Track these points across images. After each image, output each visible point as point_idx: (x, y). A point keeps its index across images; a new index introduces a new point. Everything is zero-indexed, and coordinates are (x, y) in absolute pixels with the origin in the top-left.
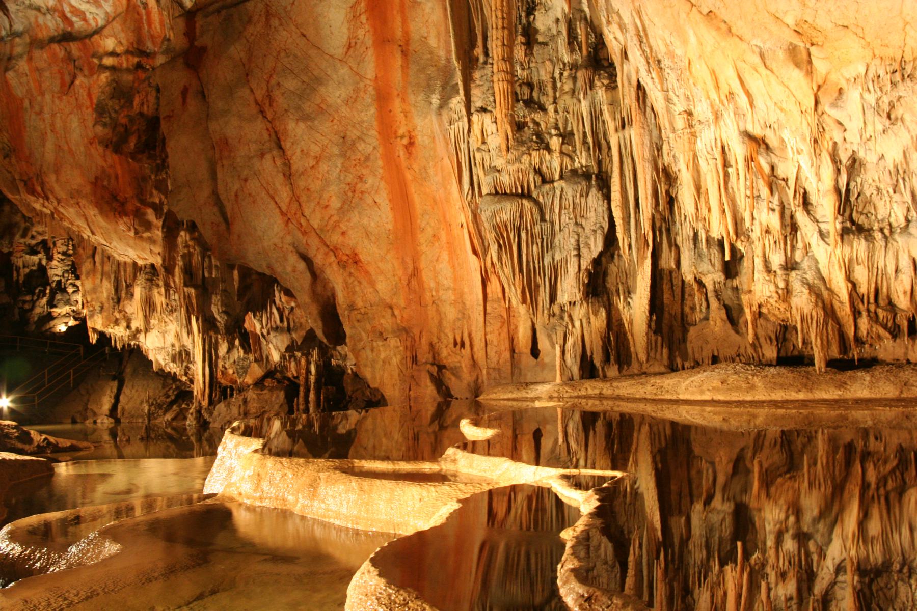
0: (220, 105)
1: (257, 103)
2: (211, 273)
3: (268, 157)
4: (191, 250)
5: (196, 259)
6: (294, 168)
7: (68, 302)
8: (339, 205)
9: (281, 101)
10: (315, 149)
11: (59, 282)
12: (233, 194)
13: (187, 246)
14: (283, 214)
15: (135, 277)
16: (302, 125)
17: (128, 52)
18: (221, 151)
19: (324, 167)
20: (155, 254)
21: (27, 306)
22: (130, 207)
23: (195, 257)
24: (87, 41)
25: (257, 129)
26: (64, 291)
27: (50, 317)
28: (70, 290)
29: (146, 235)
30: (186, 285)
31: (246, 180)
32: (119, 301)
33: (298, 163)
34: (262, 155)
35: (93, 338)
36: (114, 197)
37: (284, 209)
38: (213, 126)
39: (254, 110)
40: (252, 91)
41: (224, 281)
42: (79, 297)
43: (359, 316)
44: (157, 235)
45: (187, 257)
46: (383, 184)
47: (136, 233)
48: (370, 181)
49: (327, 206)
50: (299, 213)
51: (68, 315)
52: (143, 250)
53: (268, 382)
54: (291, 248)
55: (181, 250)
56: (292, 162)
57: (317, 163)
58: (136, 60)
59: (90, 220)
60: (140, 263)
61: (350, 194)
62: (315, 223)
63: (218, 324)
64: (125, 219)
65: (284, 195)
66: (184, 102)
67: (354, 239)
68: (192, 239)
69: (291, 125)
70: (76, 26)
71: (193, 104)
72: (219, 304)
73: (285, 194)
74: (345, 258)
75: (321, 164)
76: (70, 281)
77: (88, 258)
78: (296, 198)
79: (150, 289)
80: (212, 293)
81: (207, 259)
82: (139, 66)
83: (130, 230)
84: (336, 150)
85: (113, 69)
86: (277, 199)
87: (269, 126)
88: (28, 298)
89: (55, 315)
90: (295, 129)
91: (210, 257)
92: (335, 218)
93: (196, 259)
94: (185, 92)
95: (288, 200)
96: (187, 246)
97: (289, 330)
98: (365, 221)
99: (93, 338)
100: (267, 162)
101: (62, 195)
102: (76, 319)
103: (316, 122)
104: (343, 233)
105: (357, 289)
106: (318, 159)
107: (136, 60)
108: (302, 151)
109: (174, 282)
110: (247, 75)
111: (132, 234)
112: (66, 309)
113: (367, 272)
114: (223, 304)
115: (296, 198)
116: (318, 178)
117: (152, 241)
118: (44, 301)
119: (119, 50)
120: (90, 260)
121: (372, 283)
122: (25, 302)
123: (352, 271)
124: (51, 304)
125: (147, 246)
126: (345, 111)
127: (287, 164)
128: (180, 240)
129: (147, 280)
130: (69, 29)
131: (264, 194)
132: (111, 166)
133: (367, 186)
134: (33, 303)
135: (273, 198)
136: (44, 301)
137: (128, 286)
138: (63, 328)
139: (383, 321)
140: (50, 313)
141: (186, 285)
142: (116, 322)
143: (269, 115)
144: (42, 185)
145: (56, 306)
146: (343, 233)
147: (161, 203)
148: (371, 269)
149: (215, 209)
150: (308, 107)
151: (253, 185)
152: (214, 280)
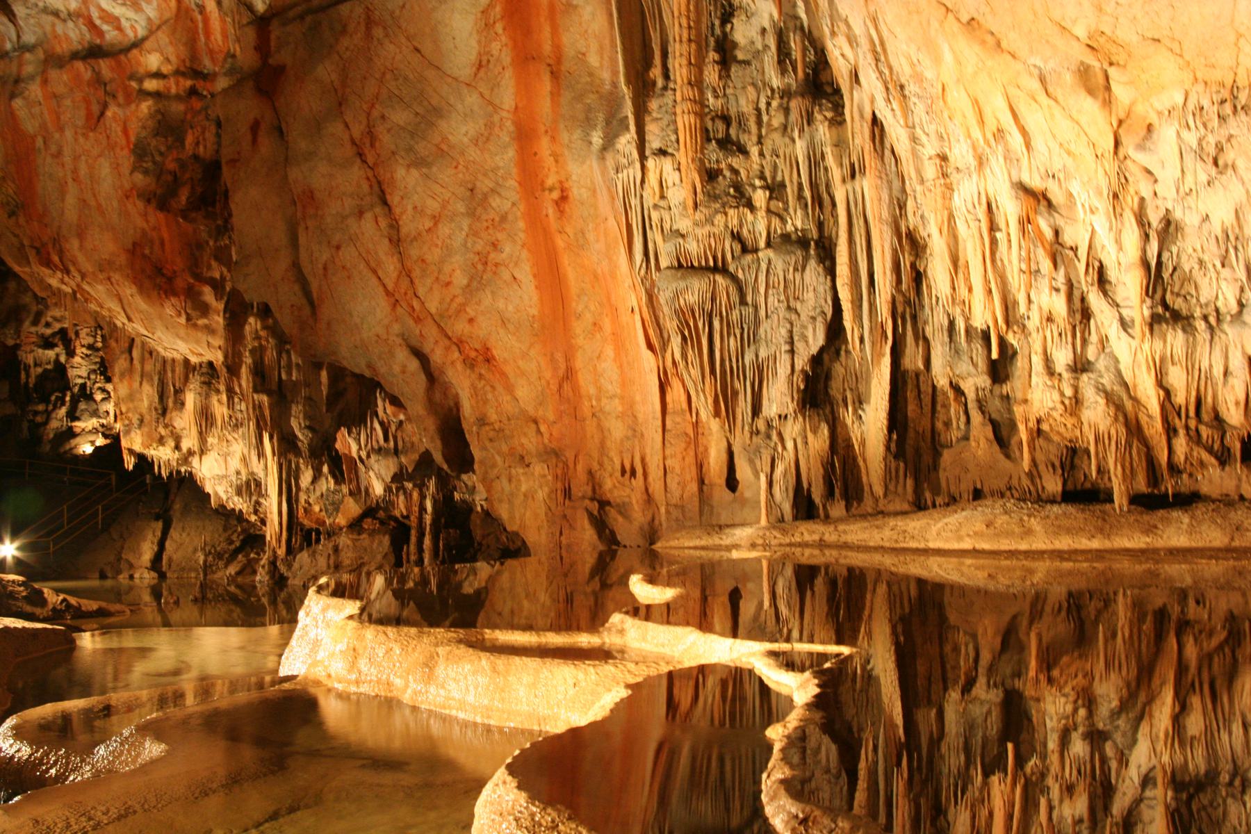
0: (303, 145)
1: (353, 142)
2: (289, 374)
3: (368, 216)
4: (264, 343)
5: (270, 355)
6: (404, 231)
7: (95, 414)
8: (465, 282)
9: (386, 140)
10: (433, 206)
11: (83, 386)
12: (320, 266)
13: (258, 338)
14: (388, 293)
15: (186, 379)
16: (415, 172)
17: (177, 73)
18: (304, 207)
19: (444, 230)
20: (214, 347)
21: (39, 419)
22: (180, 283)
23: (269, 352)
24: (122, 57)
25: (353, 178)
26: (90, 398)
27: (71, 434)
28: (99, 396)
29: (202, 322)
30: (256, 391)
31: (338, 248)
32: (164, 412)
33: (409, 225)
34: (361, 214)
35: (130, 463)
36: (159, 270)
37: (390, 287)
38: (294, 173)
39: (349, 151)
40: (347, 126)
41: (308, 385)
42: (110, 407)
43: (492, 434)
44: (218, 322)
45: (258, 353)
46: (525, 254)
47: (189, 319)
48: (508, 249)
49: (448, 284)
50: (410, 293)
51: (95, 431)
52: (198, 342)
53: (368, 523)
54: (399, 341)
55: (250, 343)
56: (401, 223)
57: (436, 224)
58: (189, 83)
59: (125, 301)
60: (194, 360)
61: (480, 267)
62: (433, 307)
63: (300, 444)
64: (174, 300)
65: (390, 267)
66: (254, 141)
67: (485, 328)
68: (264, 328)
69: (400, 172)
70: (108, 37)
71: (267, 145)
72: (301, 416)
73: (392, 268)
74: (473, 354)
75: (440, 226)
76: (97, 385)
77: (122, 352)
78: (405, 272)
79: (207, 396)
80: (292, 402)
81: (284, 356)
82: (193, 92)
83: (179, 315)
84: (461, 207)
85: (157, 95)
86: (380, 273)
87: (370, 174)
88: (41, 407)
89: (77, 430)
90: (405, 178)
91: (288, 352)
92: (460, 300)
93: (270, 355)
94: (255, 128)
95: (395, 275)
96: (258, 338)
97: (396, 452)
98: (501, 304)
99: (130, 463)
100: (367, 224)
101: (88, 267)
102: (105, 436)
103: (434, 169)
104: (471, 321)
105: (490, 396)
106: (436, 219)
107: (189, 83)
108: (415, 208)
109: (240, 386)
110: (340, 104)
111: (183, 320)
112: (92, 423)
113: (503, 374)
114: (306, 417)
115: (405, 272)
116: (437, 246)
117: (210, 330)
118: (63, 411)
119: (166, 69)
120: (126, 355)
121: (510, 389)
122: (36, 413)
123: (483, 372)
124: (73, 416)
125: (203, 337)
126: (473, 154)
127: (395, 225)
128: (247, 328)
129: (204, 383)
130: (98, 41)
131: (362, 266)
132: (154, 229)
133: (504, 255)
134: (48, 415)
135: (375, 272)
136: (63, 411)
137: (176, 392)
138: (88, 449)
139: (524, 441)
140: (71, 428)
141: (256, 391)
142: (161, 441)
143: (370, 160)
144: (61, 253)
145: (78, 419)
146: (471, 321)
147: (223, 278)
148: (508, 370)
149: (297, 287)
150: (422, 148)
151: (348, 255)
152: (295, 384)
